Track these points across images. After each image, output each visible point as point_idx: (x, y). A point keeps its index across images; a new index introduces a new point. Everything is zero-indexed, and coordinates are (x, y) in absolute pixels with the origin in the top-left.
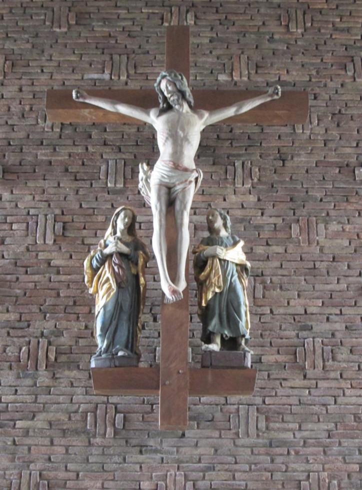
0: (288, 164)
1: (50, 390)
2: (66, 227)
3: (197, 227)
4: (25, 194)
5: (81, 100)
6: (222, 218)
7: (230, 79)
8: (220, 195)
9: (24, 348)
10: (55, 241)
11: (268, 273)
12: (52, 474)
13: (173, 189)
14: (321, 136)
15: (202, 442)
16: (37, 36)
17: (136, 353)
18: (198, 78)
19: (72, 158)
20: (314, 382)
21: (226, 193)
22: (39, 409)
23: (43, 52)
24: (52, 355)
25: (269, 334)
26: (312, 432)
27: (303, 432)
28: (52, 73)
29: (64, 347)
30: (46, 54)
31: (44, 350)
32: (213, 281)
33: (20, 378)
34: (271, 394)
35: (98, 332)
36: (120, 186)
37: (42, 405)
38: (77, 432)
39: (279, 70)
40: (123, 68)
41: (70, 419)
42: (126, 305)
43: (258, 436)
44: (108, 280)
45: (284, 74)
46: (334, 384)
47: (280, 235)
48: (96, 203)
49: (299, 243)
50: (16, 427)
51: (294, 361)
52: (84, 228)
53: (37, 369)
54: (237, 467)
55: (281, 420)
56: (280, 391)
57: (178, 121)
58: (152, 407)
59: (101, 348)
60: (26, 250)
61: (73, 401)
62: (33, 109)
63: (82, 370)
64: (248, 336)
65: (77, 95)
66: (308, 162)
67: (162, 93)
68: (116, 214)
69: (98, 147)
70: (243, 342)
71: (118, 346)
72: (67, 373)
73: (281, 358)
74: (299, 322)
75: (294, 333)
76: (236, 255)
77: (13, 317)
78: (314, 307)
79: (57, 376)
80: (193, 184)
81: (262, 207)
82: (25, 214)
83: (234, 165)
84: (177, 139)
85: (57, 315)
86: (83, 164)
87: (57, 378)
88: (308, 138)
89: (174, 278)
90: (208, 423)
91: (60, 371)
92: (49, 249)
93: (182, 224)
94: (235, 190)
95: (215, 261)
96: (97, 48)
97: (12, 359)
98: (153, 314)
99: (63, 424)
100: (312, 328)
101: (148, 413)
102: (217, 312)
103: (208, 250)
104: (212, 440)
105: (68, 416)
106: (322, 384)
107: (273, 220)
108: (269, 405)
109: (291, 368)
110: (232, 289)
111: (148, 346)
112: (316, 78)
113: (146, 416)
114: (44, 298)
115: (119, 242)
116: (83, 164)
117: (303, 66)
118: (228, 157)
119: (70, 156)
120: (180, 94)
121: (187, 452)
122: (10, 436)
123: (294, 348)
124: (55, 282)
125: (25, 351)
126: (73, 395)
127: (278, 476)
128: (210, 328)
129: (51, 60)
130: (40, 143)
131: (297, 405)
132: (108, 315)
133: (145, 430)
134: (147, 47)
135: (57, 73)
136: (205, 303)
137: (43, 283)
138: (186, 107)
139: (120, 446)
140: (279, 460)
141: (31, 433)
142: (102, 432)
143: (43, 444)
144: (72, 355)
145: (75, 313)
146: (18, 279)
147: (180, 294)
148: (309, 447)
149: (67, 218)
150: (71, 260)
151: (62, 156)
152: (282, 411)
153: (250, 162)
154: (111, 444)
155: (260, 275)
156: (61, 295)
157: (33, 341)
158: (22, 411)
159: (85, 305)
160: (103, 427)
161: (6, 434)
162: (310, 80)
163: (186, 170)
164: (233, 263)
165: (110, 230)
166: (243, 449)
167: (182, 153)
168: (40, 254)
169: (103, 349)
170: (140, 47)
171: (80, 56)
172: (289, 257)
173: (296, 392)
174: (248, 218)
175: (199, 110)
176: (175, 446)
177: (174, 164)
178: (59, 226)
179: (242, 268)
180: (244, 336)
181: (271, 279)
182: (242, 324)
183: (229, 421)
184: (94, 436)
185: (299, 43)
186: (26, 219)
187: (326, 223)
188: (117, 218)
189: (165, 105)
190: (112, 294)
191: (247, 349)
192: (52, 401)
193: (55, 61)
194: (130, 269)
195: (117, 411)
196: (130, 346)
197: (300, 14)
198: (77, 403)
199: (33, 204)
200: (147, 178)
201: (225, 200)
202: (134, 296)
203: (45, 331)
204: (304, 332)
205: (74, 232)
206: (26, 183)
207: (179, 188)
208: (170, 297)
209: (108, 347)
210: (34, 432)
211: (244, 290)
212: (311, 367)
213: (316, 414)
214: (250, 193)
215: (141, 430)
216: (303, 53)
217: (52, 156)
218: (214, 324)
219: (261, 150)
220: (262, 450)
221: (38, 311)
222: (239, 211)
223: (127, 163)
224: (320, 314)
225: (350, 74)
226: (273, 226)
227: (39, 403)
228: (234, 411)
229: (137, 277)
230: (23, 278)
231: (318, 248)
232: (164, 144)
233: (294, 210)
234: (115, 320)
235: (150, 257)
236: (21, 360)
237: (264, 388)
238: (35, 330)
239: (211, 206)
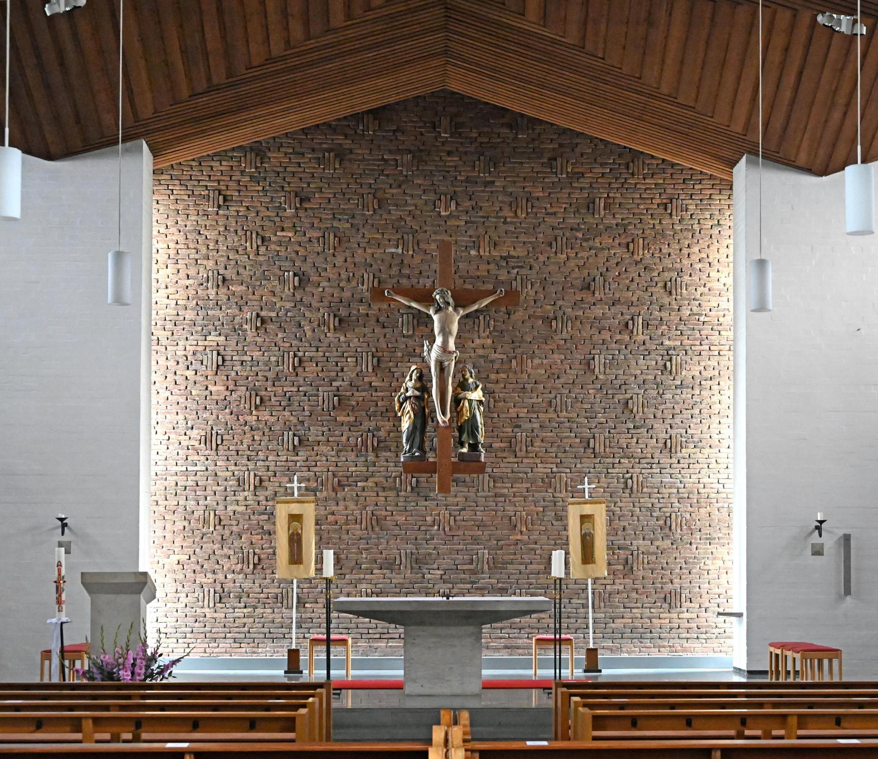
0: (511, 316)
12: (378, 513)
15: (459, 494)
35: (404, 441)
36: (411, 333)
38: (391, 489)
40: (410, 245)
42: (418, 427)
44: (409, 412)
46: (531, 461)
47: (506, 367)
54: (477, 508)
56: (502, 465)
72: (384, 454)
73: (502, 445)
75: (510, 430)
76: (477, 395)
77: (352, 419)
78: (523, 413)
89: (444, 413)
106: (525, 460)
107: (501, 356)
109: (508, 451)
121: (451, 500)
127: (499, 513)
134: (426, 228)
140: (500, 504)
149: (380, 354)
157: (365, 434)
163: (450, 352)
165: (408, 378)
173: (510, 465)
178: (375, 360)
179: (480, 402)
182: (479, 437)
187: (532, 358)
197: (524, 201)
199: (358, 344)
202: (423, 417)
205: (385, 365)
207: (446, 363)
218: (465, 437)
220: (491, 499)
225: (554, 250)
229: (424, 409)
230: (356, 394)
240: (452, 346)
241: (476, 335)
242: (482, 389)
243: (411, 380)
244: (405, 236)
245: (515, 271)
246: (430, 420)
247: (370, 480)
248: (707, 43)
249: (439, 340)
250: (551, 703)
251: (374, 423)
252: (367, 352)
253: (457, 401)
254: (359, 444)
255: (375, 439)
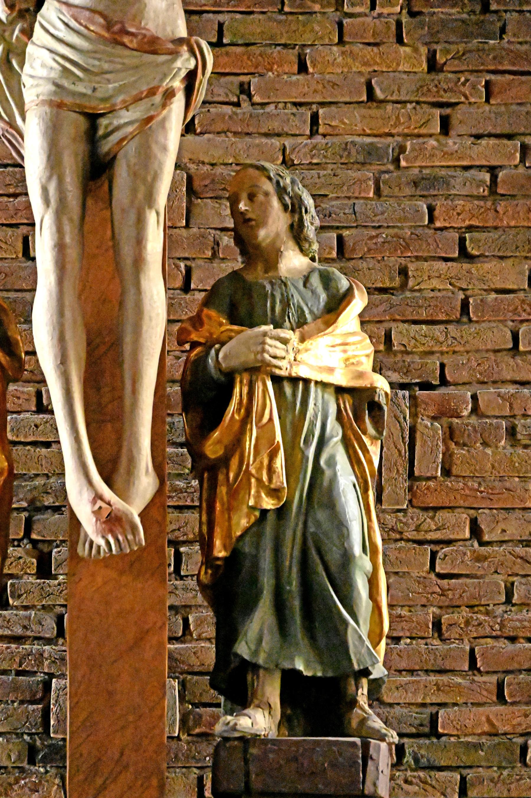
3: (197, 184)
6: (285, 207)
13: (103, 122)
25: (467, 623)
64: (378, 671)
70: (363, 698)
76: (336, 353)
80: (178, 103)
81: (445, 98)
89: (112, 466)
94: (340, 25)
102: (267, 582)
103: (234, 349)
107: (486, 152)
110: (320, 493)
128: (243, 649)
136: (225, 547)
147: (134, 529)
163: (151, 45)
179: (360, 402)
180: (366, 672)
181: (474, 397)
201: (303, 68)
211: (365, 491)
222: (357, 113)
226: (487, 177)
241: (323, 27)
250: (260, 753)
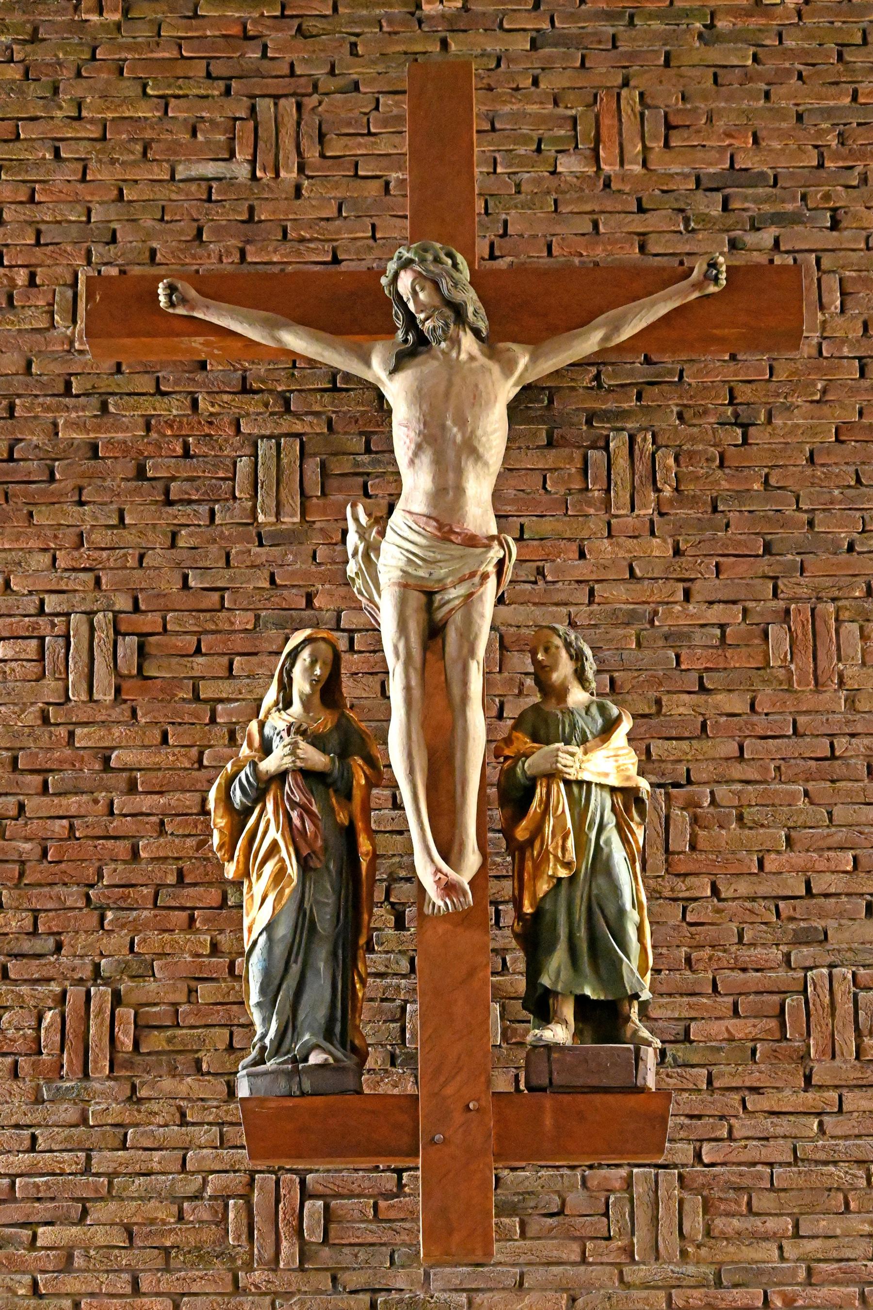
1: (126, 1134)
2: (147, 649)
3: (507, 641)
4: (30, 551)
5: (181, 311)
6: (571, 657)
7: (591, 170)
8: (569, 539)
9: (49, 1015)
10: (118, 690)
11: (704, 777)
13: (438, 597)
14: (852, 346)
16: (34, 38)
17: (354, 1050)
18: (499, 170)
19: (154, 435)
20: (834, 1095)
21: (585, 534)
22: (97, 1191)
23: (56, 91)
24: (126, 1033)
25: (710, 959)
26: (832, 1242)
27: (805, 1241)
28: (84, 163)
29: (154, 1009)
30: (64, 97)
31: (103, 1019)
32: (551, 849)
33: (44, 1101)
34: (718, 1134)
35: (254, 997)
36: (291, 520)
37: (104, 1180)
38: (200, 1255)
39: (729, 135)
41: (181, 1218)
42: (325, 923)
43: (684, 1253)
44: (274, 847)
45: (745, 150)
47: (737, 660)
48: (228, 573)
49: (790, 681)
50: (38, 1244)
51: (777, 1036)
52: (198, 651)
53: (86, 1075)
55: (744, 1208)
57: (447, 394)
58: (400, 1178)
59: (264, 1036)
60: (39, 722)
61: (188, 1167)
62: (38, 281)
63: (208, 1073)
64: (646, 995)
65: (169, 296)
66: (812, 430)
67: (404, 305)
68: (289, 654)
69: (226, 397)
71: (307, 1037)
72: (167, 1084)
73: (741, 1028)
74: (792, 919)
75: (776, 954)
76: (610, 763)
79: (143, 1093)
80: (492, 581)
82: (32, 611)
83: (606, 448)
84: (444, 475)
85: (135, 913)
86: (186, 454)
87: (140, 1101)
88: (814, 352)
89: (448, 849)
90: (550, 1221)
91: (148, 1077)
92: (103, 718)
93: (465, 699)
94: (609, 524)
95: (554, 788)
96: (209, 76)
97: (19, 1046)
98: (393, 905)
99: (162, 1234)
100: (826, 934)
101: (388, 1196)
102: (563, 932)
104: (561, 1268)
105: (175, 1209)
108: (713, 1165)
111: (383, 1000)
112: (837, 156)
113: (382, 1204)
114: (97, 864)
115: (303, 744)
116: (186, 454)
117: (800, 117)
118: (589, 422)
119: (148, 428)
120: (448, 312)
122: (24, 1273)
123: (776, 998)
124: (125, 816)
125: (51, 1025)
126: (187, 1149)
128: (546, 980)
129: (79, 118)
130: (60, 388)
131: (789, 1164)
132: (280, 950)
133: (382, 1245)
134: (355, 73)
135: (100, 161)
136: (531, 906)
137: (90, 819)
138: (468, 342)
139: (318, 1292)
141: (79, 1262)
142: (268, 1254)
143: (111, 1290)
144: (179, 1032)
145: (183, 908)
146: (21, 807)
148: (822, 1284)
149: (150, 622)
150: (164, 750)
151: (127, 429)
152: (746, 1182)
153: (649, 436)
154: (293, 1289)
155: (683, 782)
156: (143, 854)
157: (75, 994)
158: (53, 1199)
159: (210, 884)
160: (271, 1240)
161: (14, 1267)
162: (821, 166)
163: (471, 541)
164: (602, 786)
165: (271, 695)
166: (644, 1293)
167: (460, 490)
168: (78, 731)
169: (267, 1041)
170: (332, 73)
171: (162, 102)
172: (761, 725)
173: (784, 1126)
174: (648, 608)
175: (502, 345)
176: (464, 1290)
177: (440, 526)
178: (128, 645)
179: (627, 797)
181: (712, 793)
182: (631, 965)
183: (606, 1214)
184: (249, 1267)
185: (789, 43)
186: (35, 627)
188: (293, 665)
189: (410, 337)
190: (287, 891)
191: (645, 1033)
192: (130, 1170)
193: (92, 121)
194: (330, 811)
195: (305, 1194)
196: (338, 1029)
198: (198, 1172)
199: (51, 580)
200: (371, 550)
201: (582, 555)
202: (347, 882)
203: (103, 961)
204: (805, 950)
205: (169, 666)
206: (31, 514)
208: (440, 903)
209: (281, 1035)
210: (88, 1257)
211: (633, 862)
212: (823, 1053)
213: (838, 1189)
214: (652, 533)
215: (372, 1245)
216: (800, 77)
217: (98, 428)
218: (556, 969)
219: (681, 397)
221: (81, 904)
223: (309, 449)
224: (848, 895)
226: (718, 632)
227: (97, 1175)
228: (617, 1185)
229: (349, 834)
231: (843, 694)
232: (412, 462)
233: (775, 578)
234: (296, 962)
235: (379, 773)
236: (44, 1051)
237: (699, 1117)
238: (77, 961)
239: (544, 577)
240: (478, 512)
241: (596, 524)
242: (631, 738)
243: (288, 704)
244: (265, 106)
245: (766, 237)
246: (382, 916)
247: (99, 1212)
248: (734, 1215)
249: (416, 484)
251: (117, 942)
252: (90, 614)
253: (514, 795)
254: (49, 1038)
255: (126, 1013)
